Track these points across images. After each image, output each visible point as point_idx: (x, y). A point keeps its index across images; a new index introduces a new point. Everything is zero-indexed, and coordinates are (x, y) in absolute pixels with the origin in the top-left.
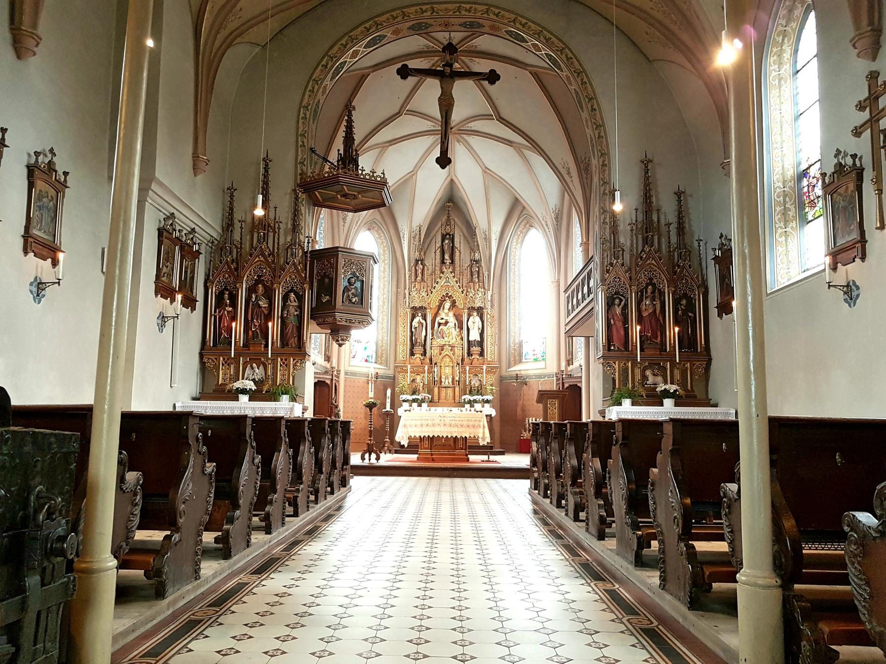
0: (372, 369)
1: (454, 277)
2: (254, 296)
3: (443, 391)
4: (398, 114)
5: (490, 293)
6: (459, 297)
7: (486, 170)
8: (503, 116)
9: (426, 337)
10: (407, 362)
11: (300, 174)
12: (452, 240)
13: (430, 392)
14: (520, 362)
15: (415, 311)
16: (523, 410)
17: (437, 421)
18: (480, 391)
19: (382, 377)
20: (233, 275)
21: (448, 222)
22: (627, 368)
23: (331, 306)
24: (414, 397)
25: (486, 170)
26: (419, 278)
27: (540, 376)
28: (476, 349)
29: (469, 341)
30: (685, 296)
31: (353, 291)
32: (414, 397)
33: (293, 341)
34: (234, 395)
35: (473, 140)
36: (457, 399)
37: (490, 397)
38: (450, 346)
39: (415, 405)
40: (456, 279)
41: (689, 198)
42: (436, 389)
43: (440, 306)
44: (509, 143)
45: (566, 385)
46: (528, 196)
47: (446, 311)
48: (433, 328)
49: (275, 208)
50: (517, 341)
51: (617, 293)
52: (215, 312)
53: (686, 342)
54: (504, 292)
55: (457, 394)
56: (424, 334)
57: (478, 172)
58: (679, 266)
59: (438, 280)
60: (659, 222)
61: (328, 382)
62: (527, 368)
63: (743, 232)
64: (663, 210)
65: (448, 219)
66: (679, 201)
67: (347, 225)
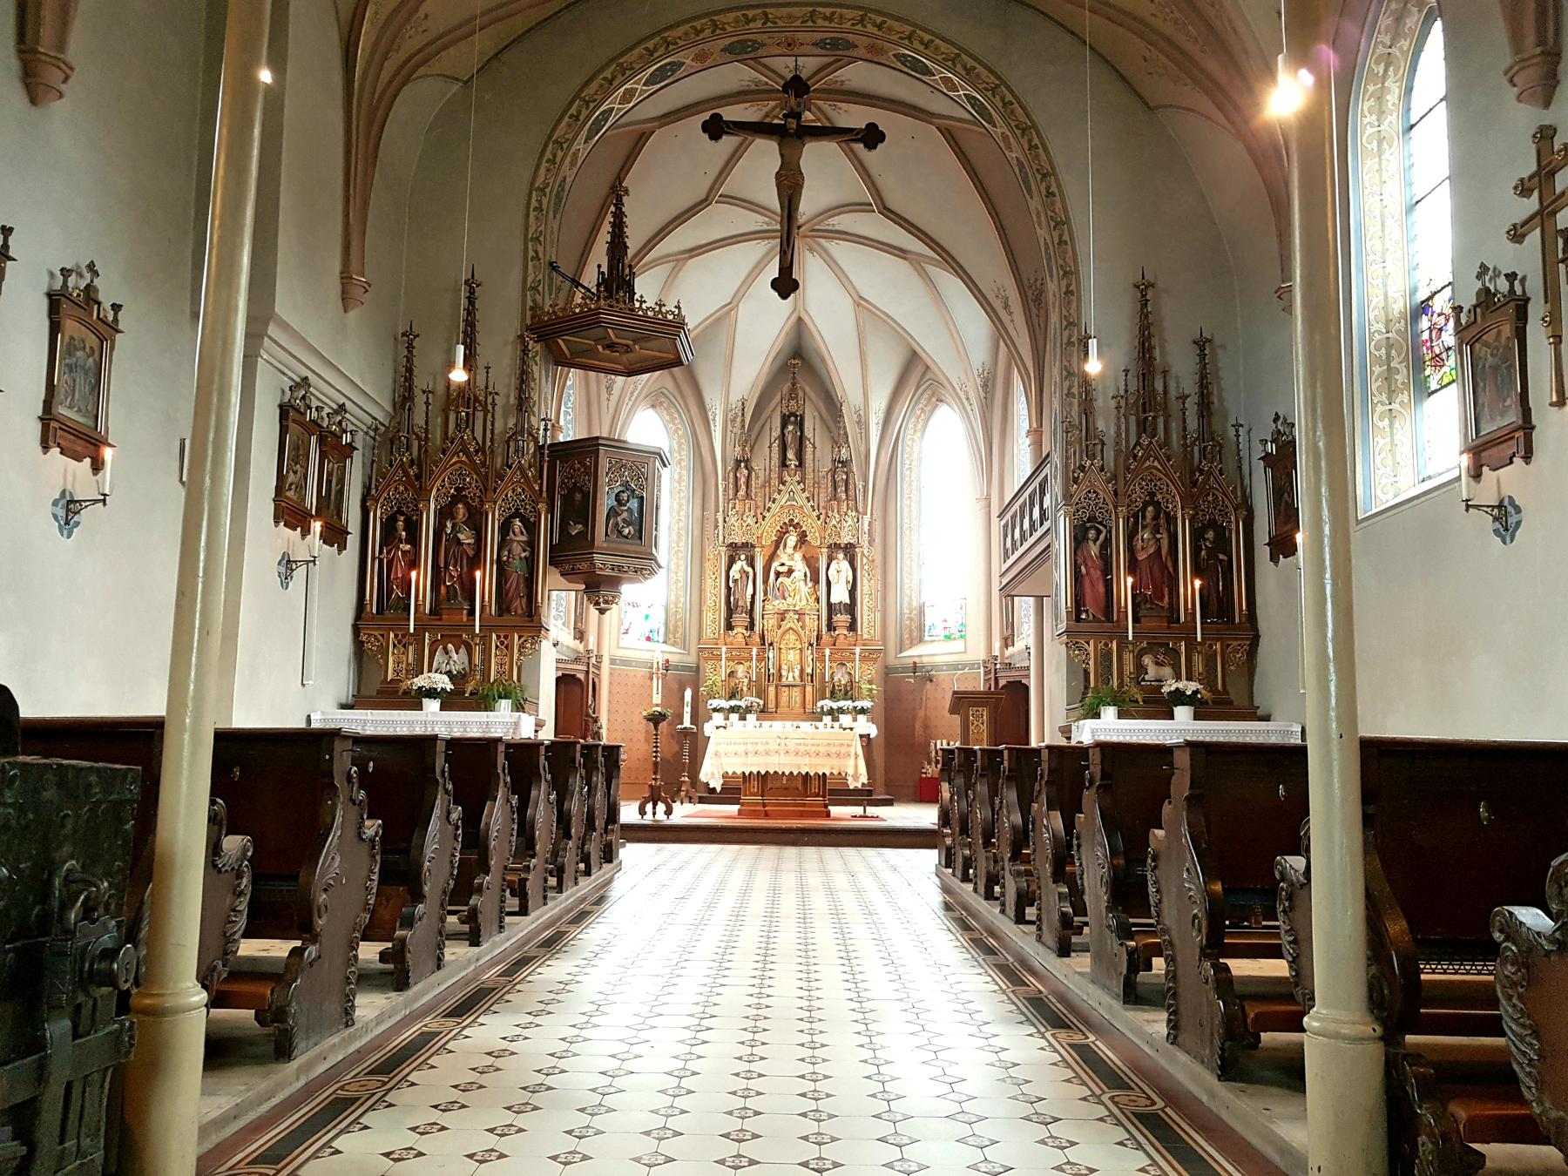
0: (659, 653)
1: (803, 490)
2: (449, 524)
3: (785, 693)
4: (704, 203)
5: (867, 519)
6: (812, 526)
7: (860, 302)
8: (890, 205)
9: (753, 596)
10: (721, 641)
11: (532, 309)
12: (801, 425)
13: (761, 693)
14: (921, 640)
15: (735, 551)
16: (926, 727)
17: (773, 746)
18: (849, 692)
19: (676, 668)
20: (413, 486)
21: (793, 394)
22: (1110, 652)
23: (585, 541)
24: (733, 703)
25: (860, 302)
26: (742, 493)
27: (955, 667)
28: (842, 619)
29: (829, 605)
30: (1213, 524)
31: (625, 515)
32: (733, 703)
33: (519, 604)
34: (414, 700)
35: (837, 248)
36: (809, 706)
37: (867, 704)
38: (796, 612)
39: (734, 717)
40: (806, 494)
41: (1219, 351)
42: (772, 690)
43: (779, 542)
44: (901, 253)
45: (1002, 683)
46: (935, 348)
47: (789, 550)
48: (766, 581)
49: (488, 368)
50: (915, 604)
51: (1092, 519)
52: (381, 552)
53: (1214, 607)
54: (891, 517)
55: (809, 697)
56: (750, 591)
57: (847, 304)
58: (1201, 472)
59: (776, 495)
60: (1165, 392)
61: (581, 676)
62: (933, 652)
63: (1314, 410)
64: (1173, 371)
65: (793, 388)
66: (1202, 356)
67: (614, 398)
